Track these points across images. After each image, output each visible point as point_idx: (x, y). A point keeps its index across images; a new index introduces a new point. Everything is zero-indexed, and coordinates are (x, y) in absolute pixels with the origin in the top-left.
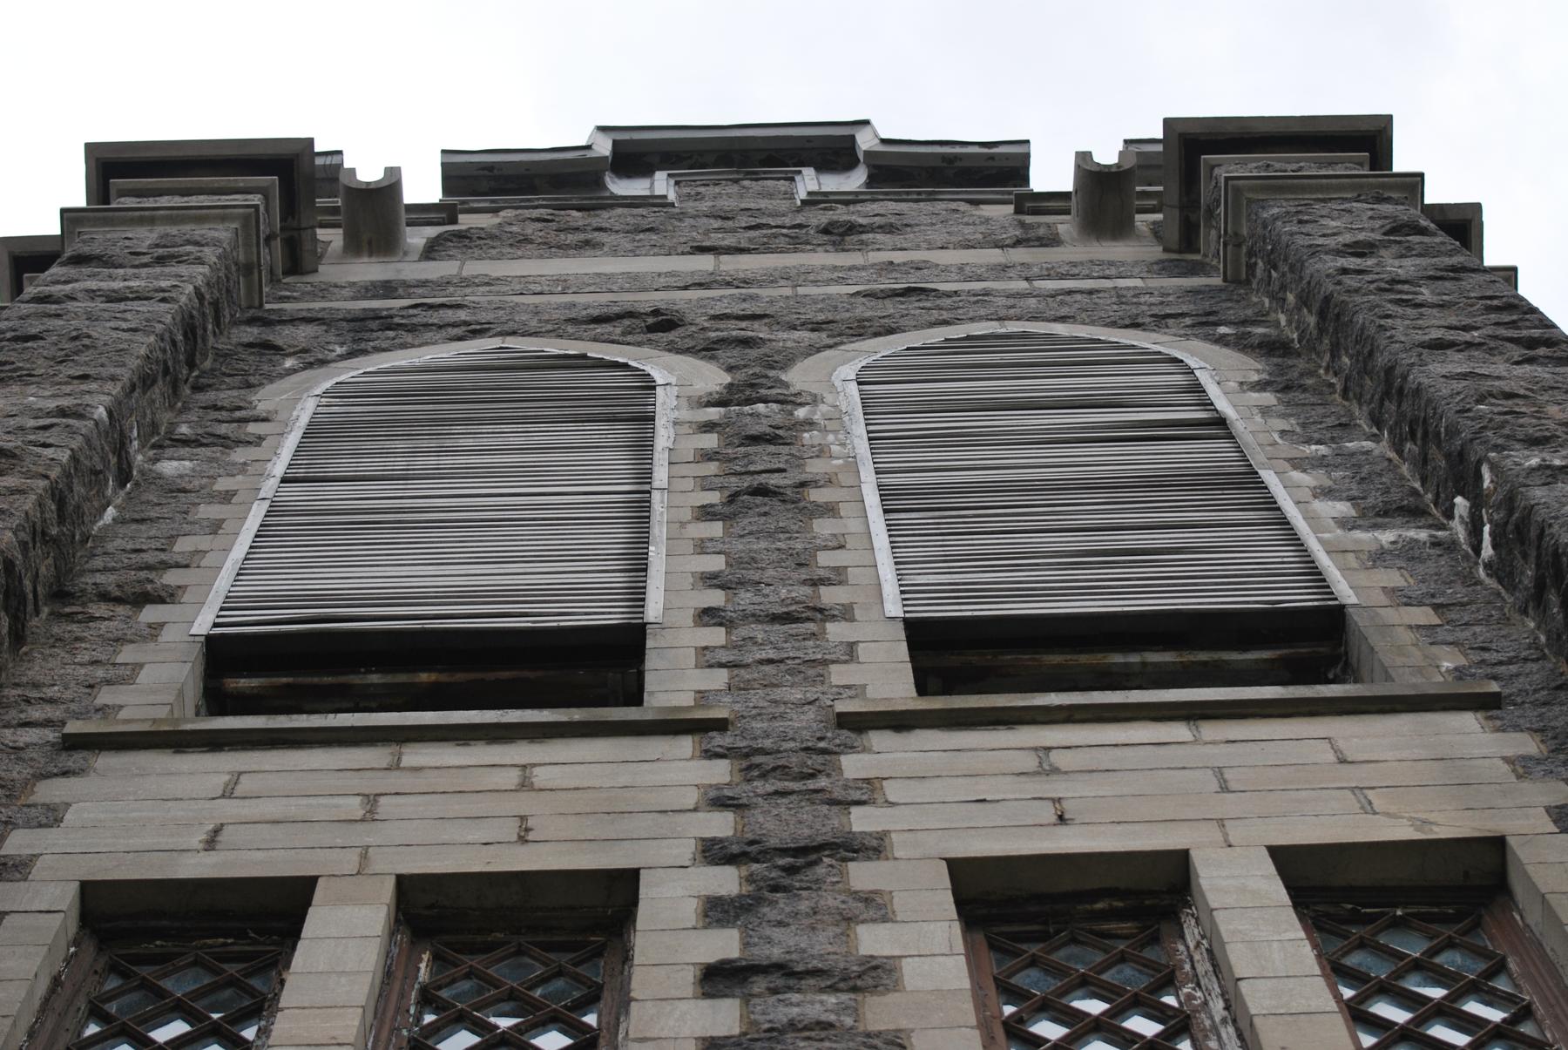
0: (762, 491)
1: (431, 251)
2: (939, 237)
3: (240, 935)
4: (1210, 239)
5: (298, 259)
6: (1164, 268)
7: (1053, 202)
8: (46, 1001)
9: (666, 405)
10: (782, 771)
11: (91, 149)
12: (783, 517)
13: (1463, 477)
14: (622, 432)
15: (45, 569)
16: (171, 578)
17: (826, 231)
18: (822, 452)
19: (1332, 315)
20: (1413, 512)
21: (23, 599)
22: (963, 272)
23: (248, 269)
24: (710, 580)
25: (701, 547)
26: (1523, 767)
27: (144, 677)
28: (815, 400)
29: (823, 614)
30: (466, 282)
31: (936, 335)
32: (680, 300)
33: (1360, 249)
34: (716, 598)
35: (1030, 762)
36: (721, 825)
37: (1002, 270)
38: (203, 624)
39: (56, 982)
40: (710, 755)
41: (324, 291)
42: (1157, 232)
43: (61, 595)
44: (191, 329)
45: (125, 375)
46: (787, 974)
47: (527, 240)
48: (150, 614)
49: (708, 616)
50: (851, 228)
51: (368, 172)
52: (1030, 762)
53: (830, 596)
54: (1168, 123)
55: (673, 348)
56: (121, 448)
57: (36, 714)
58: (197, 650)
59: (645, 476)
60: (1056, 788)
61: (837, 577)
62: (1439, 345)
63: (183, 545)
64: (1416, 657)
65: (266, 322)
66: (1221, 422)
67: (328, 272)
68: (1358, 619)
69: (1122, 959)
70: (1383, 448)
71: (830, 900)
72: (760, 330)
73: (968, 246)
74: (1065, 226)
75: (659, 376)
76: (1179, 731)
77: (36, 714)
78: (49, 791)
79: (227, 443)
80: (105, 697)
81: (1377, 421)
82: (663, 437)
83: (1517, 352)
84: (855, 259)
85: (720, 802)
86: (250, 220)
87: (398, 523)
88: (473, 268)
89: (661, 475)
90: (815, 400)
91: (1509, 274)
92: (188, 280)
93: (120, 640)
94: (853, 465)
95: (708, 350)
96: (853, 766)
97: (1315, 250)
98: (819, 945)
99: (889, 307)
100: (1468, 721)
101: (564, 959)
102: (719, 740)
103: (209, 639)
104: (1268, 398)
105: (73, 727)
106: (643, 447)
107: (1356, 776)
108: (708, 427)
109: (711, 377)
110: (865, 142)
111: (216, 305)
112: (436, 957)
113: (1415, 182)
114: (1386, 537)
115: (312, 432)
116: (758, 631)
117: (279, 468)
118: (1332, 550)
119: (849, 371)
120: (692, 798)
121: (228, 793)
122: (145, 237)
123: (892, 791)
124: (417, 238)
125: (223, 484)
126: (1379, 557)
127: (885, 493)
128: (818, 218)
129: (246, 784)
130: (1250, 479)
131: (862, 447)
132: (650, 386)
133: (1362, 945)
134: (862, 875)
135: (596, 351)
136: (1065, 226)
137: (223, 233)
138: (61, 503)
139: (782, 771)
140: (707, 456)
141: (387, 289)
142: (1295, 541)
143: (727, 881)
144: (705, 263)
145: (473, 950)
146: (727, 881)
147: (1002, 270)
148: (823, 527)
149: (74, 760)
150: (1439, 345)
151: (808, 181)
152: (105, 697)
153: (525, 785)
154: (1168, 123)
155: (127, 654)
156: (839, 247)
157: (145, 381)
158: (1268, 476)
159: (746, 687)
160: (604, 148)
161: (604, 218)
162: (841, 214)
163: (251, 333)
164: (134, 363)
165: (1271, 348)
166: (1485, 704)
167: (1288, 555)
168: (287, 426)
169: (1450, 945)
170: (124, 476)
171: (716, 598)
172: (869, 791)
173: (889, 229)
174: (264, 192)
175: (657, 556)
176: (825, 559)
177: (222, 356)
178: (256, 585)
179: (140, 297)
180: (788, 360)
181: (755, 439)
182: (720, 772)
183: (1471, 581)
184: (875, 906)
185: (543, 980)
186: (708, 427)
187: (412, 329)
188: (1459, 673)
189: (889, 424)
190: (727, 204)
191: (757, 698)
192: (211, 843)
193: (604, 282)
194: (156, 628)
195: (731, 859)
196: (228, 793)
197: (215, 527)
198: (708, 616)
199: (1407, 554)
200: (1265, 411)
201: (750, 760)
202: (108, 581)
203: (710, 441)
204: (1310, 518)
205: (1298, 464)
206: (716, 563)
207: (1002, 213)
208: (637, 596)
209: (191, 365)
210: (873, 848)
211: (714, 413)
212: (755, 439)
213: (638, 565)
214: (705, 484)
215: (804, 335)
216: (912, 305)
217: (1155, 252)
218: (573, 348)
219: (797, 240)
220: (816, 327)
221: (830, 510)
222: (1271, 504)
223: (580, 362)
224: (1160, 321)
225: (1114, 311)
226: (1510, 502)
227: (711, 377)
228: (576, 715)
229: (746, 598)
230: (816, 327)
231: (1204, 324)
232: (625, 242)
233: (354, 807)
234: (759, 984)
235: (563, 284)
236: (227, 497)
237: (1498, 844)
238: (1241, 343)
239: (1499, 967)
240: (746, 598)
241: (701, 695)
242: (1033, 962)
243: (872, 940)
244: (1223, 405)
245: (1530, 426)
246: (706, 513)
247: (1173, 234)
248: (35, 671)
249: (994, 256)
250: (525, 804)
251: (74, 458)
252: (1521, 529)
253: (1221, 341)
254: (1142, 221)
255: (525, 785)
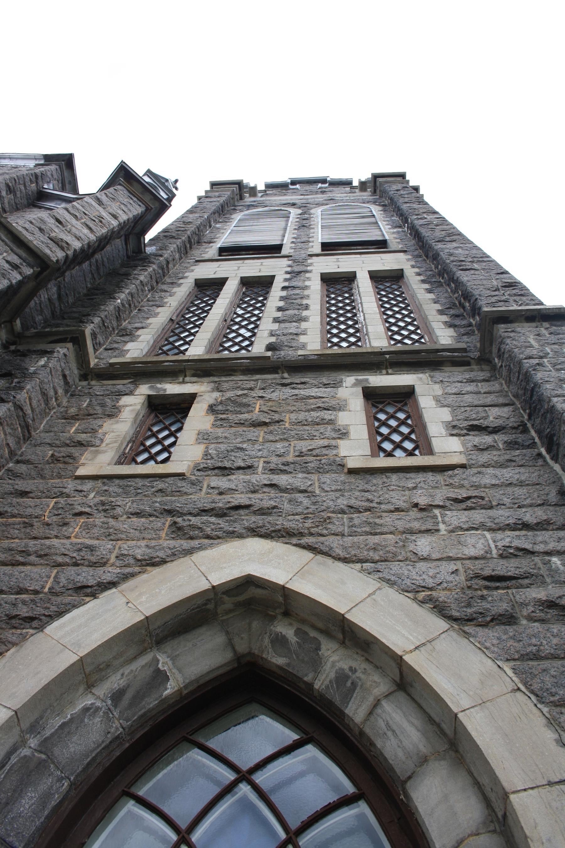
0: (304, 226)
1: (262, 196)
2: (337, 192)
3: (218, 286)
4: (378, 191)
5: (241, 198)
6: (371, 196)
7: (355, 187)
8: (188, 295)
9: (292, 216)
10: (299, 262)
11: (210, 182)
12: (306, 229)
13: (406, 221)
14: (285, 219)
15: (196, 239)
16: (215, 240)
17: (321, 192)
18: (314, 221)
19: (391, 199)
20: (400, 227)
21: (191, 242)
22: (340, 197)
23: (233, 198)
24: (294, 238)
25: (293, 234)
26: (408, 260)
27: (209, 253)
28: (314, 214)
29: (309, 242)
30: (266, 200)
31: (334, 205)
32: (297, 201)
33: (397, 190)
34: (294, 240)
35: (335, 260)
36: (289, 269)
37: (347, 196)
38: (219, 246)
39: (190, 292)
40: (289, 260)
41: (245, 202)
42: (371, 191)
43: (199, 242)
44: (222, 206)
45: (210, 212)
46: (294, 287)
47: (276, 194)
48: (211, 244)
49: (293, 242)
50: (325, 191)
51: (252, 185)
52: (335, 260)
53: (311, 239)
54: (372, 174)
55: (294, 208)
56: (210, 222)
57: (192, 258)
58: (217, 249)
59: (287, 225)
60: (338, 263)
61: (313, 237)
62: (406, 203)
63: (218, 236)
64: (396, 246)
65: (235, 206)
66: (374, 216)
67: (246, 200)
68: (388, 241)
69: (345, 287)
70: (398, 219)
71: (302, 278)
72: (308, 205)
73: (342, 193)
74: (357, 190)
75: (292, 212)
76: (358, 256)
77: (192, 258)
78: (192, 268)
79: (226, 222)
80: (203, 255)
81: (397, 215)
82: (291, 219)
83: (417, 203)
84: (325, 196)
85: (289, 266)
86: (233, 191)
87: (250, 231)
88: (268, 198)
89: (289, 224)
90: (314, 214)
91: (422, 195)
92: (222, 200)
93: (206, 248)
94: (318, 223)
95: (300, 208)
96: (309, 261)
97: (390, 191)
98: (300, 284)
99: (328, 202)
100: (402, 254)
101: (264, 288)
102: (290, 258)
103: (219, 248)
104: (382, 212)
105: (197, 259)
106: (287, 221)
107: (382, 261)
108: (298, 218)
109: (300, 211)
110: (328, 179)
111: (227, 203)
112: (246, 288)
113: (408, 182)
114: (395, 230)
115: (239, 220)
116: (299, 244)
117: (234, 225)
118: (386, 232)
119: (320, 210)
120: (285, 266)
121: (218, 267)
122: (217, 194)
123: (314, 264)
124: (260, 195)
125: (225, 228)
126: (394, 233)
127: (322, 226)
128: (320, 190)
129: (221, 266)
130: (377, 223)
131: (320, 220)
132: (290, 213)
133: (381, 284)
134: (307, 275)
135: (283, 208)
136: (357, 190)
137: (229, 193)
138: (198, 229)
139: (299, 262)
140: (297, 222)
141: (255, 201)
142: (381, 231)
143: (288, 276)
144: (302, 197)
145: (251, 287)
146: (288, 276)
147: (347, 196)
148: (312, 231)
149: (197, 263)
150: (406, 203)
151: (320, 185)
152: (203, 255)
153: (262, 265)
154: (372, 174)
155: (207, 250)
156: (323, 194)
157: (214, 213)
158: (379, 223)
159: (296, 251)
160: (289, 181)
161: (288, 191)
162: (324, 190)
163: (233, 208)
164: (212, 210)
165: (383, 206)
166: (405, 252)
167: (380, 233)
168: (236, 219)
169: (394, 284)
170: (210, 226)
171: (294, 240)
172: (311, 264)
173: (331, 191)
174: (236, 187)
175: (287, 235)
176: (311, 235)
177: (228, 211)
178: (228, 240)
179: (214, 202)
180: (311, 209)
181: (304, 219)
182: (290, 262)
183: (407, 236)
184: (309, 279)
185: (261, 291)
186: (298, 218)
187: (257, 206)
188: (402, 248)
189: (324, 217)
190: (307, 189)
191: (298, 253)
192: (215, 273)
193: (287, 200)
194: (212, 246)
195: (289, 273)
196: (218, 267)
197: (223, 233)
198: (293, 242)
199: (398, 232)
200: (381, 214)
201: (294, 261)
202: (206, 241)
203: (298, 220)
204: (385, 228)
205: (384, 221)
206: (295, 236)
207: (348, 189)
208: (283, 240)
209: (223, 212)
210: (310, 272)
211: (299, 216)
212: (304, 219)
213: (284, 236)
214: (296, 225)
215: (314, 206)
216: (331, 201)
217: (370, 194)
218: (279, 208)
219: (317, 193)
220: (316, 204)
221: (313, 228)
222: (379, 226)
223: (281, 210)
224: (368, 202)
225: (361, 201)
226: (412, 223)
227: (300, 211)
228: (270, 255)
229: (298, 240)
230: (316, 204)
231: (374, 203)
232: (291, 194)
233: (236, 268)
234: (290, 289)
235: (280, 200)
236: (225, 229)
237: (402, 270)
238: (379, 205)
239: (401, 287)
240: (298, 240)
241: (289, 253)
242: (332, 287)
243: (307, 283)
244: (375, 213)
245: (417, 213)
246: (295, 229)
247: (373, 191)
248: (193, 253)
249: (346, 195)
250: (261, 267)
251: (201, 223)
252: (413, 227)
253: (377, 205)
254: (369, 190)
255: (262, 265)
